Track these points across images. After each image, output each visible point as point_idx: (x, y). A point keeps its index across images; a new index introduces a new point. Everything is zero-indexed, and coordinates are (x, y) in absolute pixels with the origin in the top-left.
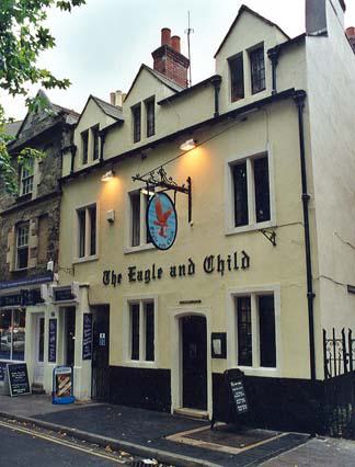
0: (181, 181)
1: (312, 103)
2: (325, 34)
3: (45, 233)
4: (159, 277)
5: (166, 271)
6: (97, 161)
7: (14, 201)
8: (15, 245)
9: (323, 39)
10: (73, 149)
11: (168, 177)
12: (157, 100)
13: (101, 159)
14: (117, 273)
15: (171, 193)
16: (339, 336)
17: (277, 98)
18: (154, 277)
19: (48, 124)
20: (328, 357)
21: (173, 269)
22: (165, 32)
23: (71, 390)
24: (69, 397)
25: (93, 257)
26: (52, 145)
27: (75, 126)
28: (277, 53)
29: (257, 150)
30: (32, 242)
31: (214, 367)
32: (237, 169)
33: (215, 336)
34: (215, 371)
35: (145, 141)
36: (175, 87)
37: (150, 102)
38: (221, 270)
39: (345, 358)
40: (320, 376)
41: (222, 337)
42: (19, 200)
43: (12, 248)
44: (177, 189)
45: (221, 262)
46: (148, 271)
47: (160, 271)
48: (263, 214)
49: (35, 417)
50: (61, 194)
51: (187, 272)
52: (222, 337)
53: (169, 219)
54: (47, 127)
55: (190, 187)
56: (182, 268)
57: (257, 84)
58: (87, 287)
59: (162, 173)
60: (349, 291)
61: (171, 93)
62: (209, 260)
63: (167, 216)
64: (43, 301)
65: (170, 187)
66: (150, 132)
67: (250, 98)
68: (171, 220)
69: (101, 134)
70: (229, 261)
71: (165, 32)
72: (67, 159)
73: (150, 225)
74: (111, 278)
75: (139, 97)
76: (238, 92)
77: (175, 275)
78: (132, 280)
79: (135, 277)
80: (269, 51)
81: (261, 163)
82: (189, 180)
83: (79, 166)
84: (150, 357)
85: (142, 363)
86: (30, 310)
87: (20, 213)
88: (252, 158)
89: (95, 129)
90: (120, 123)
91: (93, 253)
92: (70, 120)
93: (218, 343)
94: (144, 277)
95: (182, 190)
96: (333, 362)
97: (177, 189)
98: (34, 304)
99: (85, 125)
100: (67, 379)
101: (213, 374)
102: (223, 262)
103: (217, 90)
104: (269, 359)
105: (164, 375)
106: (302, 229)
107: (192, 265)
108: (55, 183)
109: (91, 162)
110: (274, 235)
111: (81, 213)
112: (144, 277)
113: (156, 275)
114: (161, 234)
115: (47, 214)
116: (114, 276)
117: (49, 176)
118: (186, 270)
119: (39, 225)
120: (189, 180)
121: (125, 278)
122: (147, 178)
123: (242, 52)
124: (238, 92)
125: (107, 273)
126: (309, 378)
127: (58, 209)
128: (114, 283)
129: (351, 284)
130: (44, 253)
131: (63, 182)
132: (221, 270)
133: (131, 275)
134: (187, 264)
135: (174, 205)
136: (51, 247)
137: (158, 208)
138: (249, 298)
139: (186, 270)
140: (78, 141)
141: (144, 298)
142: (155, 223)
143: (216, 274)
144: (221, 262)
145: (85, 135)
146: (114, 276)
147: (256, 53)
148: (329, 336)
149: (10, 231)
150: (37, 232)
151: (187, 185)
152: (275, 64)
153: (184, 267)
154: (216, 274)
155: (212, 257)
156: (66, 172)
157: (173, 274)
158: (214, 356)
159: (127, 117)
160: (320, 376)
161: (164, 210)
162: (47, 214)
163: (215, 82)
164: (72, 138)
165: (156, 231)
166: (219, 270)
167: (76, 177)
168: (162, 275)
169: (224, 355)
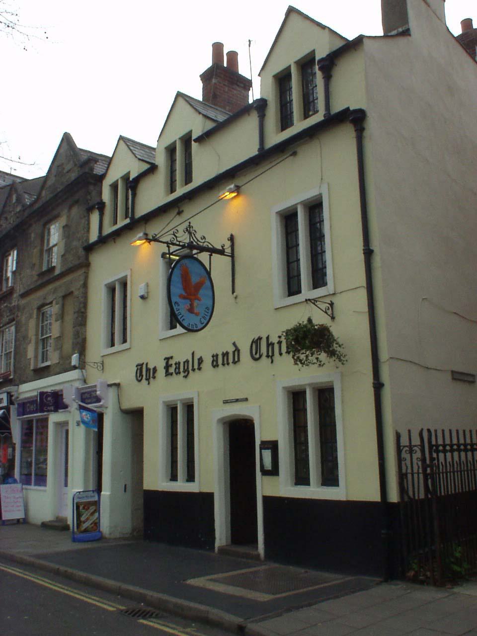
0: (218, 240)
1: (372, 125)
2: (406, 33)
3: (70, 318)
4: (199, 369)
5: (208, 360)
6: (128, 221)
7: (36, 278)
8: (37, 335)
9: (402, 41)
10: (101, 206)
11: (199, 236)
12: (194, 136)
13: (132, 218)
14: (151, 366)
15: (204, 257)
16: (416, 441)
17: (334, 121)
18: (193, 370)
19: (73, 176)
20: (404, 471)
21: (215, 357)
22: (218, 48)
23: (97, 524)
24: (93, 533)
25: (126, 346)
26: (77, 202)
27: (102, 177)
28: (330, 64)
29: (310, 194)
30: (55, 331)
31: (265, 487)
32: (288, 219)
33: (265, 445)
34: (268, 494)
35: (180, 191)
36: (211, 114)
37: (187, 140)
38: (270, 356)
39: (425, 470)
40: (394, 496)
41: (273, 446)
42: (42, 274)
43: (33, 338)
44: (213, 251)
45: (270, 345)
46: (187, 361)
47: (201, 361)
48: (319, 280)
49: (38, 557)
50: (87, 265)
51: (231, 360)
52: (273, 446)
53: (201, 292)
54: (73, 178)
55: (233, 250)
56: (225, 355)
57: (308, 107)
58: (118, 385)
59: (189, 230)
60: (454, 379)
61: (210, 125)
62: (257, 342)
63: (199, 286)
64: (65, 407)
65: (202, 249)
66: (188, 179)
67: (299, 125)
68: (204, 292)
69: (132, 184)
70: (280, 343)
71: (218, 48)
72: (95, 217)
73: (174, 299)
74: (144, 373)
75: (175, 135)
76: (285, 121)
77: (217, 366)
78: (168, 374)
79: (172, 370)
80: (320, 61)
81: (315, 207)
82: (232, 239)
83: (108, 229)
84: (191, 478)
85: (181, 486)
86: (54, 418)
87: (40, 293)
88: (302, 203)
89: (126, 178)
90: (153, 168)
91: (125, 341)
92: (99, 169)
93: (267, 455)
94: (182, 369)
95: (221, 252)
96: (410, 476)
97: (213, 251)
98: (56, 410)
99: (114, 175)
100: (92, 509)
101: (266, 499)
102: (273, 344)
103: (262, 117)
104: (330, 477)
105: (208, 498)
106: (363, 294)
107: (237, 350)
108: (81, 252)
109: (122, 222)
110: (332, 304)
111: (111, 289)
112: (182, 369)
113: (196, 366)
114: (191, 310)
115: (72, 293)
116: (148, 370)
117: (75, 243)
118: (223, 360)
119: (63, 306)
120: (232, 239)
121: (161, 372)
122: (167, 238)
123: (290, 66)
124: (285, 121)
125: (140, 367)
126: (376, 497)
127: (85, 285)
128: (148, 379)
129: (454, 369)
130: (68, 345)
131: (90, 248)
132: (270, 356)
133: (167, 367)
134: (231, 349)
135: (209, 273)
136: (77, 334)
137: (185, 278)
138: (304, 392)
139: (223, 360)
140: (106, 196)
141: (181, 398)
142: (181, 296)
143: (265, 361)
144: (270, 345)
145: (114, 187)
146: (148, 370)
147: (306, 64)
148: (404, 441)
149: (31, 317)
150: (61, 316)
151: (228, 244)
152: (328, 78)
153: (227, 353)
154: (265, 361)
155: (260, 339)
156: (94, 237)
157: (215, 365)
158: (265, 472)
159: (161, 160)
160: (394, 496)
161: (194, 280)
162: (72, 293)
163: (261, 105)
164: (101, 193)
165: (182, 308)
166: (268, 356)
167: (104, 240)
168: (203, 366)
169: (274, 471)
